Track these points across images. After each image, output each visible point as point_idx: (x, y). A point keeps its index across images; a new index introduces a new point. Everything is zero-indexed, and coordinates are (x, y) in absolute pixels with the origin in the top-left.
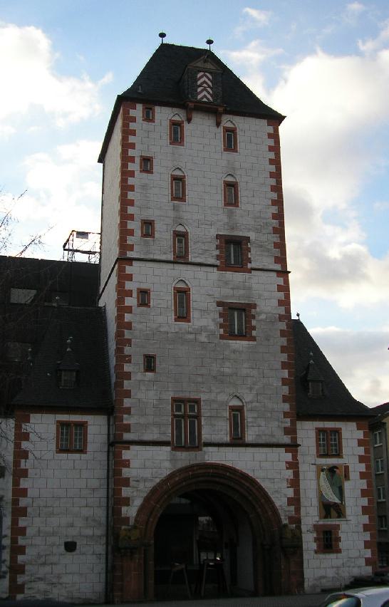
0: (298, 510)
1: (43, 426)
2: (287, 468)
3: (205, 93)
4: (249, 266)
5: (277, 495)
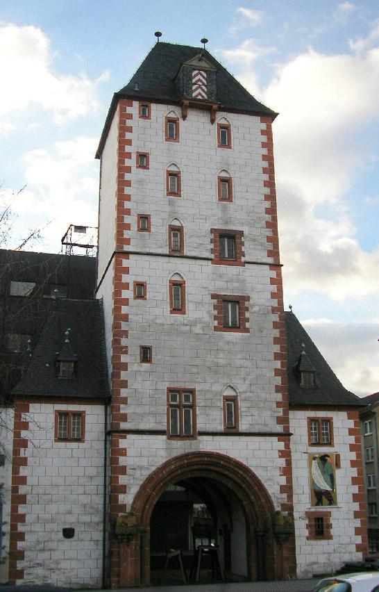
0: (290, 497)
1: (42, 416)
2: (280, 457)
3: (199, 90)
4: (243, 259)
5: (270, 483)
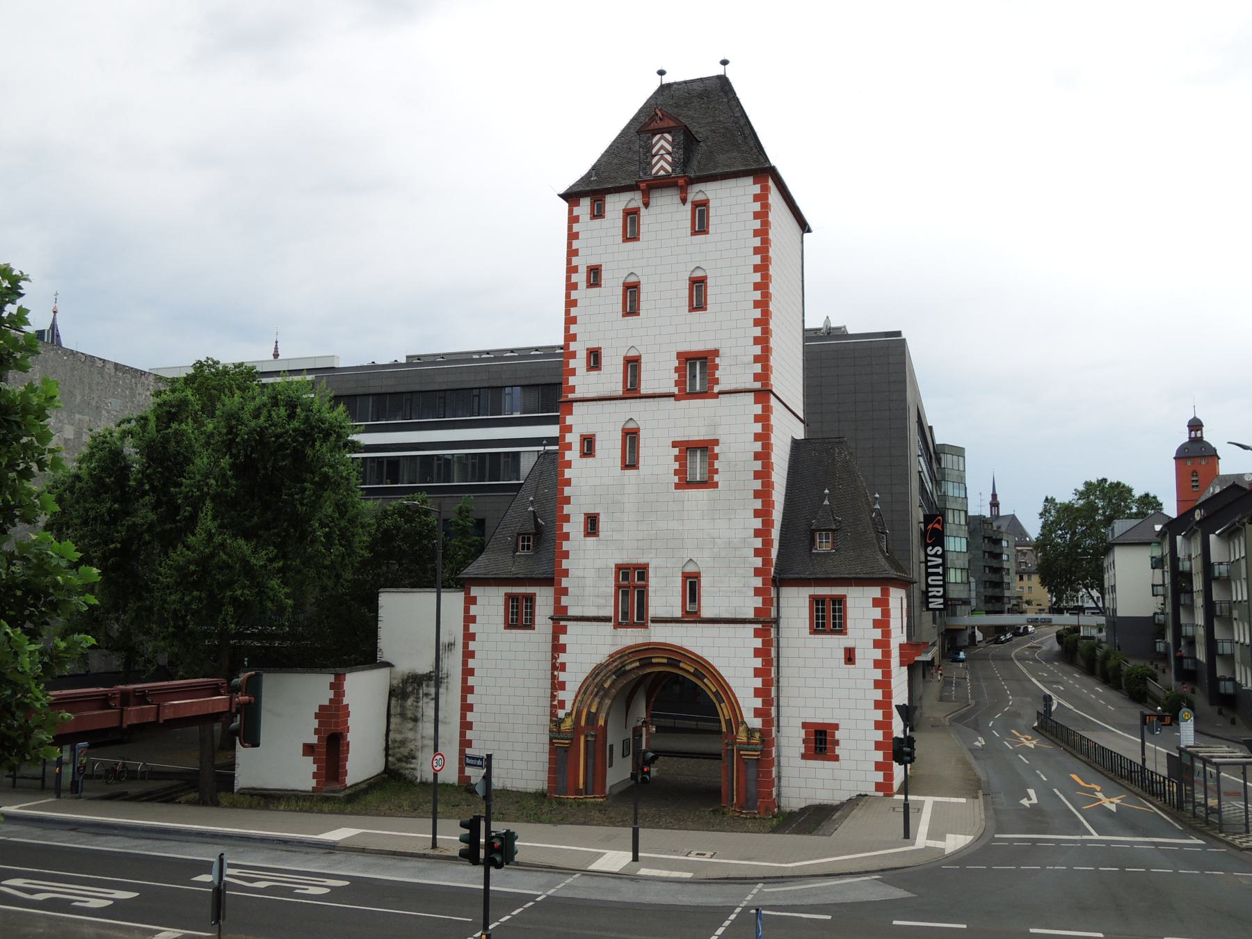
1: (491, 602)
3: (662, 163)
4: (716, 389)
